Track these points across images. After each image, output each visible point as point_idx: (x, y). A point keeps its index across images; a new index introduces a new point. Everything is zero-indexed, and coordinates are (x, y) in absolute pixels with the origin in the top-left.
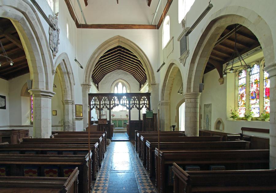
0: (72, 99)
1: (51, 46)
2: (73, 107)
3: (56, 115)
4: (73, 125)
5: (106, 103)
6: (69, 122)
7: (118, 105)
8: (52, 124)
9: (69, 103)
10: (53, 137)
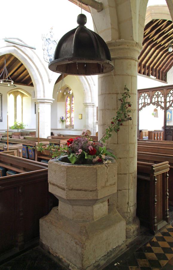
0: (92, 101)
1: (45, 60)
2: (93, 110)
3: (82, 119)
4: (94, 130)
5: (146, 101)
6: (88, 126)
7: (148, 104)
8: (51, 127)
9: (89, 106)
10: (93, 144)
